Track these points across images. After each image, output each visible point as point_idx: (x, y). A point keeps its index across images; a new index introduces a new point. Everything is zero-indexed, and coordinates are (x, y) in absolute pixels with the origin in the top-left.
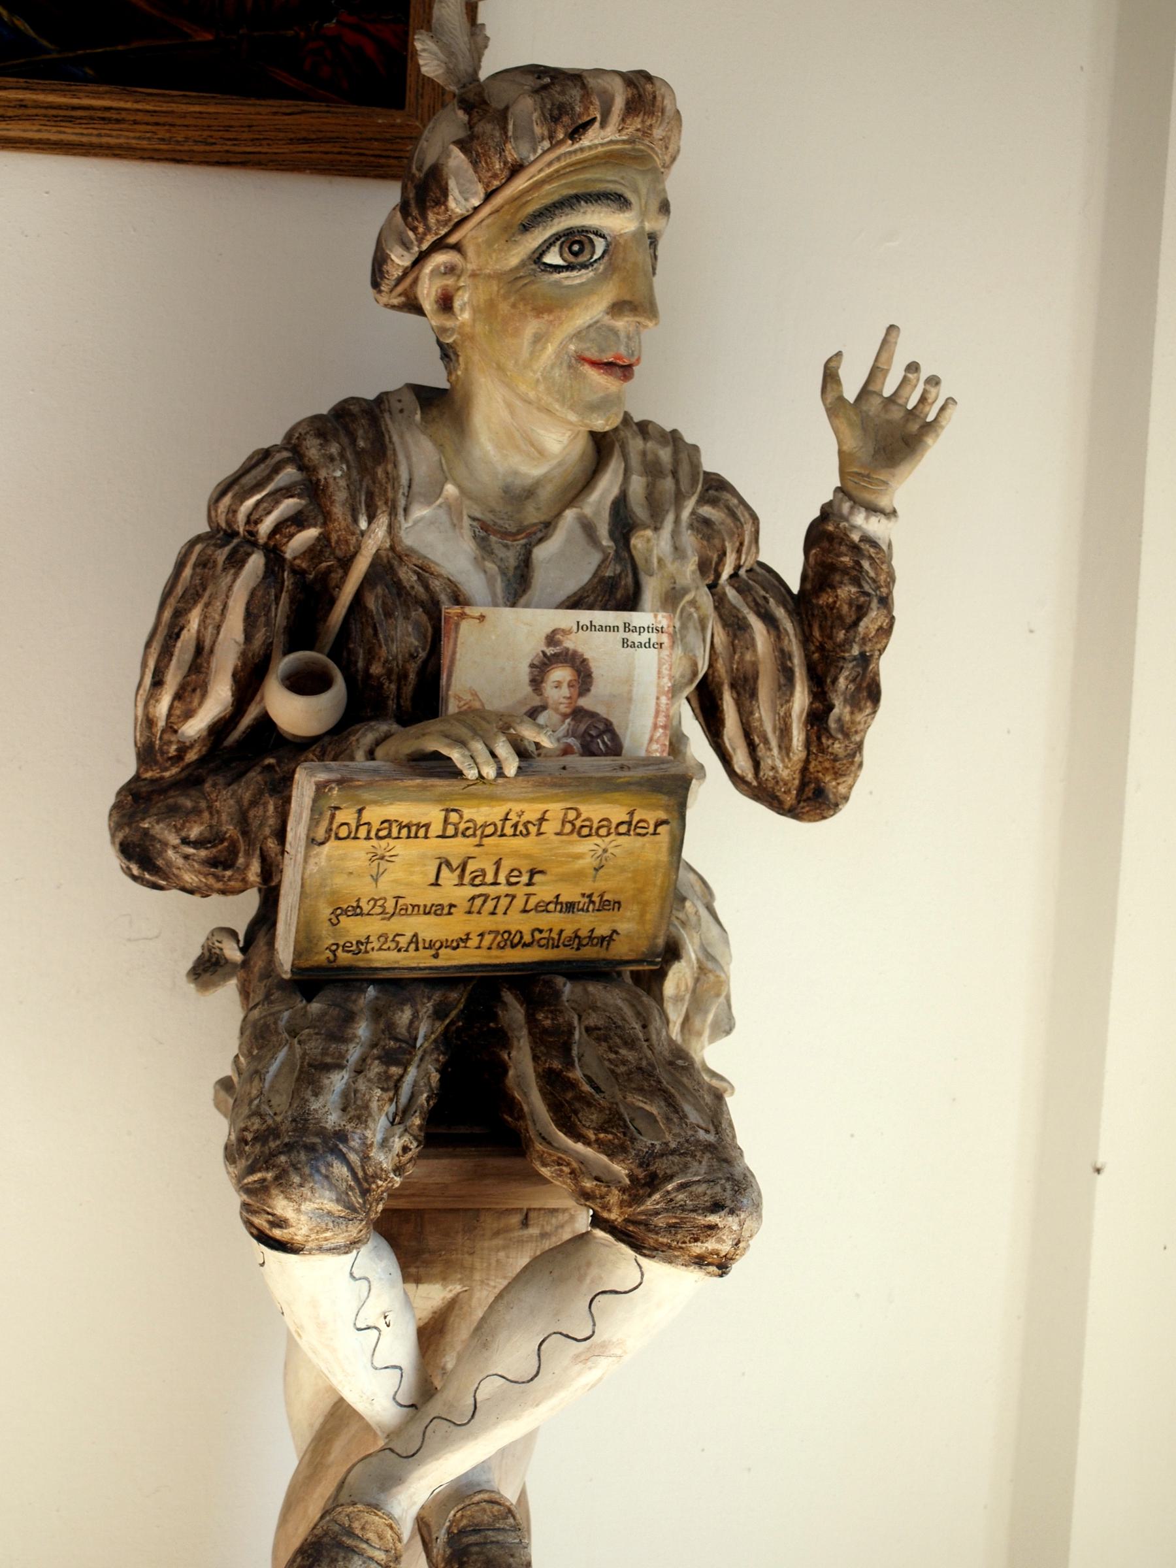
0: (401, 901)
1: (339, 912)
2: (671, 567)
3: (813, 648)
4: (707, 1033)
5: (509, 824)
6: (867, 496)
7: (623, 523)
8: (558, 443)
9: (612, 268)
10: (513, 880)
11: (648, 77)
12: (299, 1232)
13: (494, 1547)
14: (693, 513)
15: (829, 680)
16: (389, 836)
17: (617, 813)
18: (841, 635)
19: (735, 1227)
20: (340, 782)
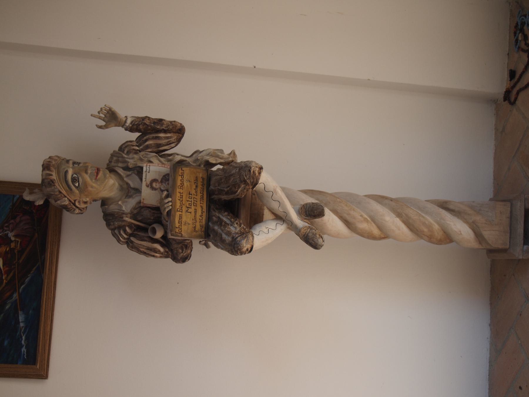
1: (195, 231)
2: (136, 160)
6: (123, 122)
8: (112, 181)
11: (43, 165)
17: (180, 178)
18: (149, 127)
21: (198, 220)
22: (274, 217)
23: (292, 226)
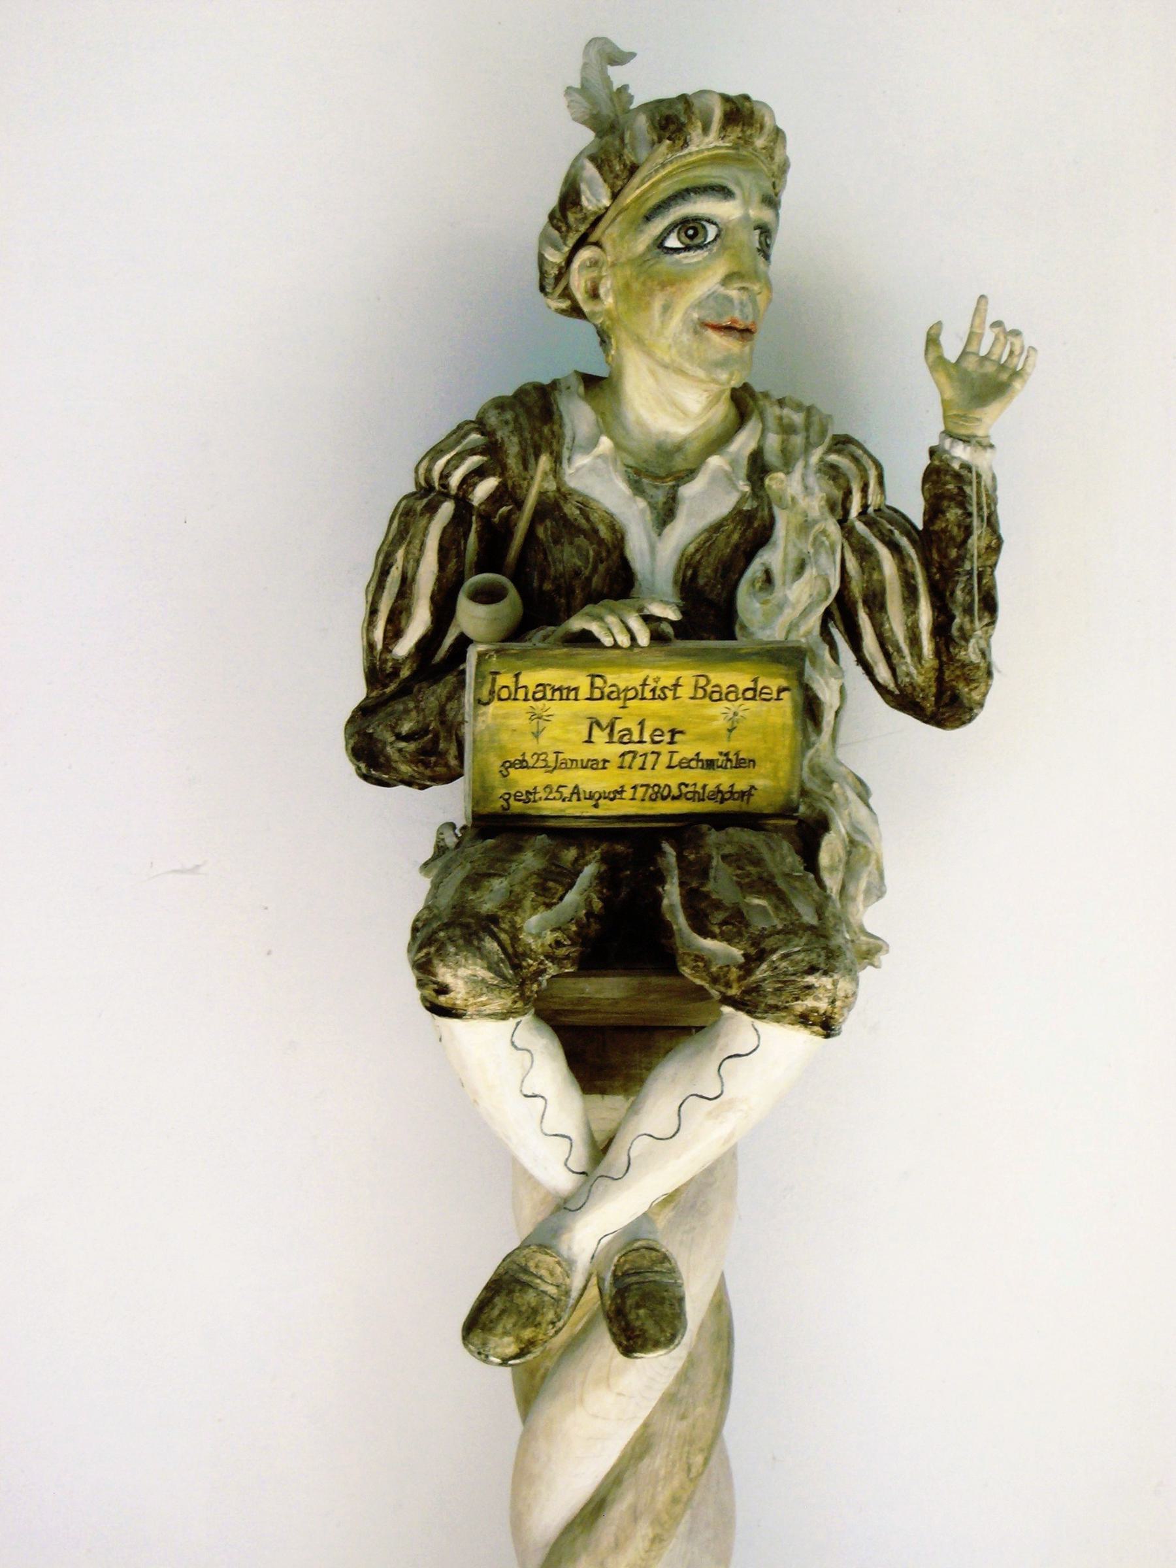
0: (561, 756)
1: (508, 765)
3: (935, 570)
4: (860, 898)
5: (647, 689)
7: (758, 468)
9: (724, 248)
10: (657, 739)
11: (784, 138)
12: (459, 996)
13: (652, 1285)
14: (821, 460)
15: (948, 594)
16: (543, 698)
17: (744, 682)
18: (954, 553)
19: (829, 987)
20: (497, 651)
21: (557, 778)
22: (600, 1137)
23: (566, 1208)
